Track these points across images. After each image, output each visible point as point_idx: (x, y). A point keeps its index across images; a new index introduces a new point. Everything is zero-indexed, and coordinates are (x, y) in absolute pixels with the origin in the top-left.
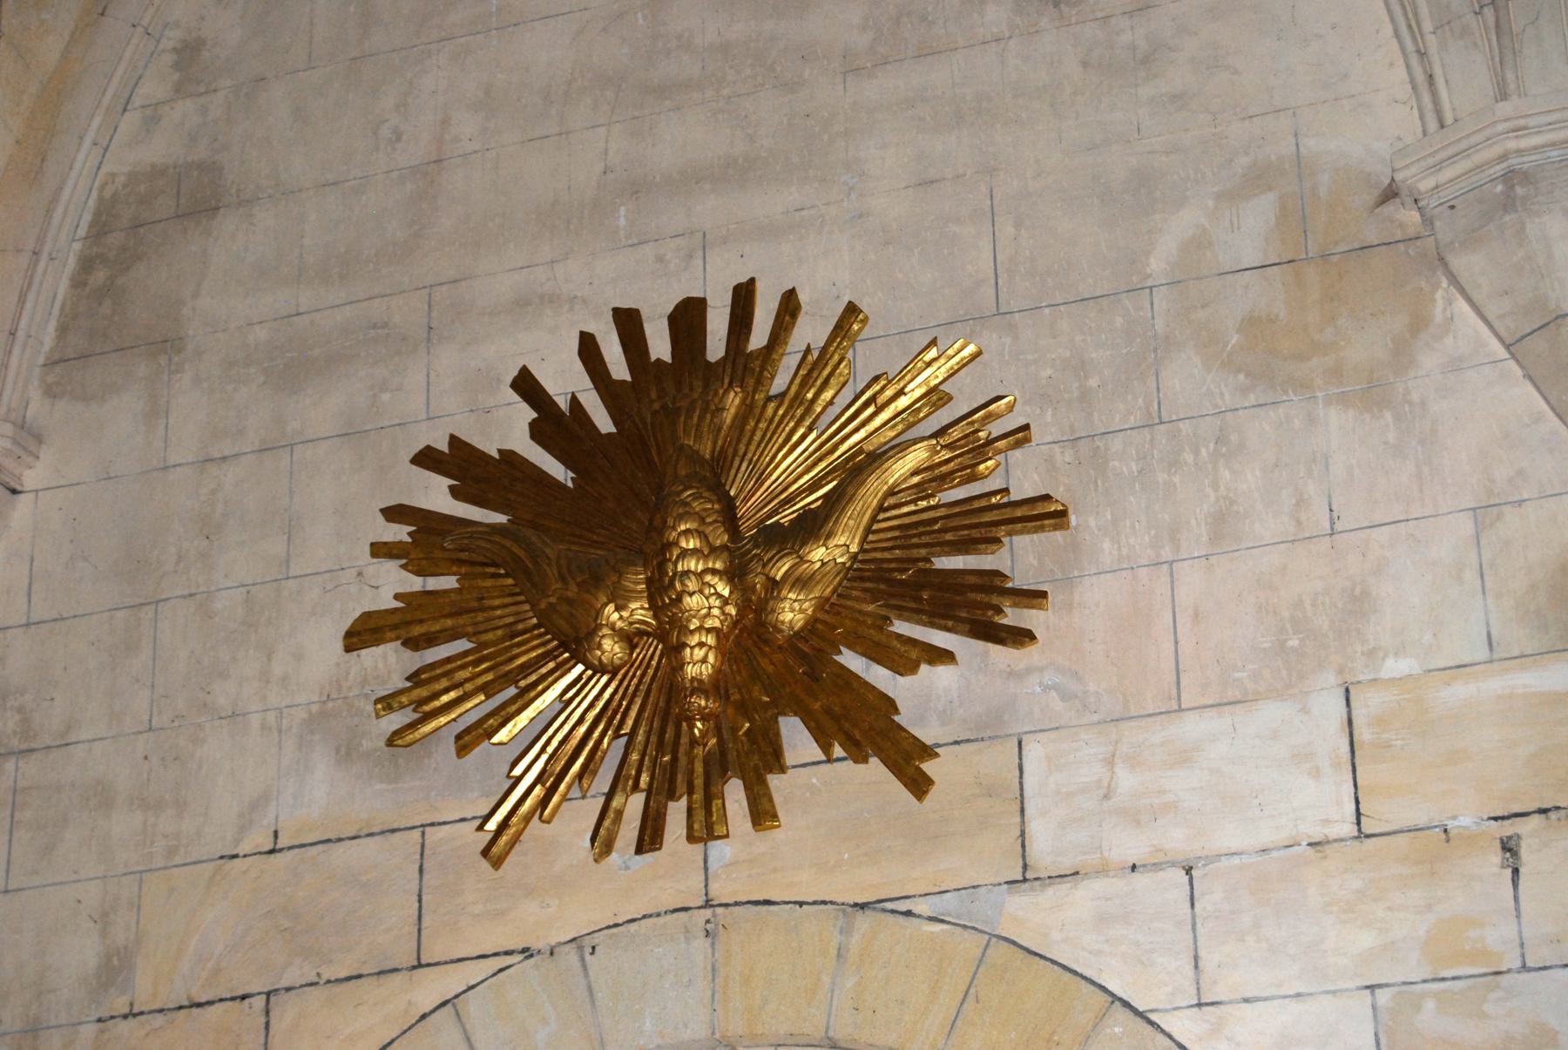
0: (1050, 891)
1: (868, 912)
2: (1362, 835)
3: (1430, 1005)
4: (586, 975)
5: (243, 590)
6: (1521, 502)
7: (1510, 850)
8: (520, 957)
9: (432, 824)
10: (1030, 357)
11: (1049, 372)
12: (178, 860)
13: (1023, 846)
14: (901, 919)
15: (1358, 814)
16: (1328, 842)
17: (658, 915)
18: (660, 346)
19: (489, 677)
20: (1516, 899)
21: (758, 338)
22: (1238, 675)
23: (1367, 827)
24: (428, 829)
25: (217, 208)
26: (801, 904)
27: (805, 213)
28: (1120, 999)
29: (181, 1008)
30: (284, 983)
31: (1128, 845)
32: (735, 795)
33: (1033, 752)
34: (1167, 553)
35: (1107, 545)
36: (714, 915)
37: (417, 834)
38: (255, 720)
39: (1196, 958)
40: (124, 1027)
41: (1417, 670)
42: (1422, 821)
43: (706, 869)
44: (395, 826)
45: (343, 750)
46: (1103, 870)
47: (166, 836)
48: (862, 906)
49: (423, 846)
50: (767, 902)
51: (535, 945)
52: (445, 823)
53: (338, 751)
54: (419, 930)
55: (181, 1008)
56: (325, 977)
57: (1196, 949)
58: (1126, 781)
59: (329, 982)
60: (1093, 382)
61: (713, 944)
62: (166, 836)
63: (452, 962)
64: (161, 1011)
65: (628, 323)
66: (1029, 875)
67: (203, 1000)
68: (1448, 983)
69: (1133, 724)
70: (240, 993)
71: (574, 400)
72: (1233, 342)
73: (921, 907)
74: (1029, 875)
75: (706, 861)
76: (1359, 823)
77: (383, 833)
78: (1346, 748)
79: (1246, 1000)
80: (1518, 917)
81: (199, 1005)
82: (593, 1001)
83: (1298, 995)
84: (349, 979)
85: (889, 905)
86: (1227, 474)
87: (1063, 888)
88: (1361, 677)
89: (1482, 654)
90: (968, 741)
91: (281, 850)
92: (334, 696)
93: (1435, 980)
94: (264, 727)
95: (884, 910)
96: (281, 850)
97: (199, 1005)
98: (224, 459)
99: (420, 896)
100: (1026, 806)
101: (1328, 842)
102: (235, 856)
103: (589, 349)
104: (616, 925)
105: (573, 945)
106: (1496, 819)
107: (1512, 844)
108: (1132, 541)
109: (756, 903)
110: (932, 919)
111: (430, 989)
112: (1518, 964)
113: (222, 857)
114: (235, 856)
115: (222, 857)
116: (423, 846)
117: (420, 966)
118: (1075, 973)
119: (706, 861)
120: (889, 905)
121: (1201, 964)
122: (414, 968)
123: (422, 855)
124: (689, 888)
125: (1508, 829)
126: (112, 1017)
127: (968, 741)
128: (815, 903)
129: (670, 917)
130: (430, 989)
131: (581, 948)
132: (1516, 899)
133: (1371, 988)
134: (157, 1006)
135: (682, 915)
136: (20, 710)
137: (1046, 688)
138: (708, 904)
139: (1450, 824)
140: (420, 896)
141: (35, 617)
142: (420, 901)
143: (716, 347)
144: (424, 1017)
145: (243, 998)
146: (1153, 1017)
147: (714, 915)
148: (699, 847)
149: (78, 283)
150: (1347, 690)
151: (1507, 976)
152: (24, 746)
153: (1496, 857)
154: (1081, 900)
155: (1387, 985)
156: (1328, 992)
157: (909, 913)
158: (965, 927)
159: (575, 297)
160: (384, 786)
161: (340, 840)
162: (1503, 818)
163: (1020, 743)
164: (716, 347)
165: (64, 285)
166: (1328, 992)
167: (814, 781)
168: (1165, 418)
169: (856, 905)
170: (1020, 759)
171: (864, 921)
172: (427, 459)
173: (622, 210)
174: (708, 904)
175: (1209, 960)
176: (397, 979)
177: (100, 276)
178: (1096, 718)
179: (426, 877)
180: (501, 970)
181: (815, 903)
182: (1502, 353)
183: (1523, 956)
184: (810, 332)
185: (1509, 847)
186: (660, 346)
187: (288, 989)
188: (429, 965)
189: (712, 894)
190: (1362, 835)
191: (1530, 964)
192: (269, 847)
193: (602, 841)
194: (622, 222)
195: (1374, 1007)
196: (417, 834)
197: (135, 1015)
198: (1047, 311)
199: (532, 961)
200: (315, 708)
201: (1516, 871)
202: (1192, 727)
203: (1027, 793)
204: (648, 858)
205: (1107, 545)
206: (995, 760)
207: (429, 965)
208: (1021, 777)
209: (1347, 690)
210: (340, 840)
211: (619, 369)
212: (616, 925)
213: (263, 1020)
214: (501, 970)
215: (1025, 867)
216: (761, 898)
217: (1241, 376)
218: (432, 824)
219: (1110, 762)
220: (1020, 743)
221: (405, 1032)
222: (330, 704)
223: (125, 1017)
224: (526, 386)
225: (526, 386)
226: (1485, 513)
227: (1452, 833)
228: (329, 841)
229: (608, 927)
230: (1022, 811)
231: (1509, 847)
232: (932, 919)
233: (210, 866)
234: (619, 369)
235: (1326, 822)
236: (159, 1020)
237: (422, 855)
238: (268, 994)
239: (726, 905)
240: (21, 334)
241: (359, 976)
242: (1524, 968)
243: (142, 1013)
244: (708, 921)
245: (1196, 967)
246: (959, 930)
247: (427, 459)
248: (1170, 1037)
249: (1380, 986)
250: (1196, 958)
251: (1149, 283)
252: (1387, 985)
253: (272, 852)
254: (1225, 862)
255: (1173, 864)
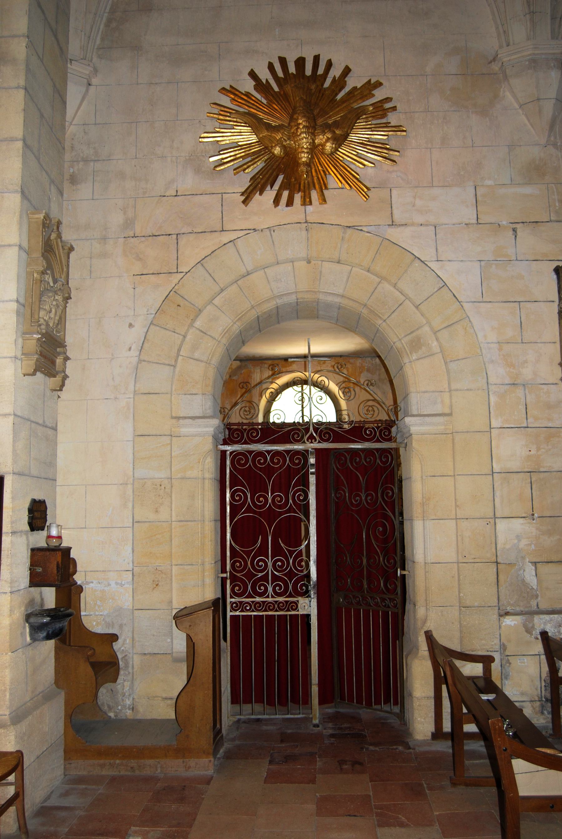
0: (399, 229)
1: (350, 229)
2: (478, 223)
3: (494, 266)
4: (272, 238)
5: (164, 122)
6: (520, 146)
7: (515, 231)
8: (253, 231)
9: (225, 193)
10: (393, 88)
11: (399, 93)
12: (147, 196)
13: (392, 216)
14: (360, 232)
15: (477, 218)
16: (470, 224)
17: (292, 224)
18: (292, 69)
19: (243, 154)
20: (515, 243)
21: (321, 71)
22: (448, 179)
23: (480, 221)
24: (223, 194)
25: (151, 10)
26: (332, 225)
27: (331, 39)
28: (418, 257)
29: (150, 236)
30: (182, 232)
31: (419, 219)
32: (314, 195)
33: (394, 192)
34: (429, 146)
35: (414, 141)
36: (308, 225)
37: (220, 195)
38: (169, 159)
39: (437, 249)
40: (132, 240)
41: (493, 184)
42: (493, 221)
43: (305, 213)
44: (213, 192)
45: (197, 170)
46: (413, 224)
47: (143, 189)
48: (349, 227)
49: (222, 198)
50: (322, 223)
51: (257, 229)
52: (228, 193)
53: (195, 170)
54: (222, 221)
55: (150, 236)
56: (195, 231)
57: (437, 247)
58: (418, 202)
59: (196, 233)
60: (411, 98)
61: (308, 233)
62: (143, 189)
63: (233, 230)
64: (144, 236)
65: (283, 61)
66: (394, 224)
67: (157, 234)
68: (499, 262)
69: (420, 188)
70: (168, 233)
71: (267, 80)
72: (448, 93)
73: (365, 229)
74: (394, 224)
75: (305, 211)
76: (477, 220)
77: (210, 194)
78: (475, 201)
79: (449, 261)
80: (516, 247)
81: (155, 236)
82: (274, 245)
83: (462, 261)
84: (202, 232)
85: (356, 228)
86: (446, 128)
87: (402, 228)
88: (479, 184)
89: (509, 182)
90: (377, 188)
91: (179, 196)
92: (193, 155)
93: (495, 260)
94: (172, 161)
95: (355, 229)
96: (179, 196)
97: (155, 236)
98: (156, 84)
99: (222, 212)
100: (393, 206)
101: (470, 224)
102: (165, 196)
103: (271, 67)
104: (280, 225)
105: (268, 229)
106: (511, 223)
107: (515, 229)
108: (420, 141)
109: (320, 223)
110: (368, 232)
111: (226, 237)
112: (515, 259)
113: (160, 196)
114: (165, 196)
115: (160, 196)
116: (222, 198)
117: (223, 231)
118: (406, 250)
119: (305, 211)
120: (356, 228)
121: (438, 251)
122: (221, 231)
123: (222, 201)
124: (301, 217)
125: (514, 226)
126: (129, 237)
127: (377, 188)
128: (336, 225)
129: (295, 224)
130: (226, 237)
131: (270, 231)
132: (515, 243)
133: (480, 261)
134: (143, 235)
135: (299, 224)
136: (94, 148)
137: (397, 176)
138: (306, 222)
139: (500, 223)
140: (222, 212)
141: (97, 122)
142: (222, 213)
143: (308, 71)
144: (225, 244)
145: (169, 235)
146: (426, 262)
147: (308, 225)
148: (304, 207)
149: (107, 25)
150: (475, 187)
151: (512, 262)
152: (96, 159)
153: (511, 232)
154: (408, 231)
155: (484, 261)
156: (469, 261)
157: (361, 230)
158: (377, 235)
159: (264, 52)
160: (210, 181)
161: (197, 195)
162: (513, 223)
163: (391, 190)
164: (308, 71)
165: (102, 27)
166: (469, 261)
167: (335, 193)
168: (430, 110)
169: (347, 226)
170: (391, 193)
171: (349, 231)
172: (223, 90)
173: (277, 30)
174: (306, 222)
175: (440, 250)
176: (216, 234)
177: (114, 25)
178: (411, 186)
179: (223, 207)
180: (247, 234)
181: (336, 225)
182: (517, 107)
183: (517, 257)
184: (336, 72)
185: (514, 230)
186: (292, 69)
187: (183, 234)
188: (226, 231)
189: (307, 219)
190: (478, 223)
191: (518, 259)
192: (176, 194)
193: (276, 202)
194: (277, 33)
195: (481, 266)
196: (220, 195)
197: (136, 237)
198: (399, 77)
199: (256, 232)
200: (187, 158)
201: (516, 236)
202: (436, 191)
203: (393, 203)
204: (289, 208)
205: (414, 141)
206: (384, 193)
207: (226, 231)
208: (391, 198)
209: (475, 187)
210: (197, 195)
211: (280, 74)
212: (280, 225)
213: (176, 241)
214: (247, 234)
215: (393, 222)
216: (321, 222)
217: (450, 103)
218: (225, 193)
219: (415, 198)
220: (391, 190)
221: (219, 248)
222: (192, 157)
223: (133, 237)
224: (253, 75)
225: (253, 75)
226: (511, 147)
227: (501, 225)
228: (194, 194)
229: (278, 225)
230: (392, 207)
231: (514, 230)
232: (368, 232)
233: (157, 198)
234: (280, 74)
235: (469, 219)
236: (143, 239)
237: (222, 201)
238: (177, 235)
239: (311, 223)
240: (91, 37)
241: (205, 232)
242: (517, 260)
243: (138, 237)
244: (306, 227)
245: (437, 251)
246: (375, 236)
247: (223, 90)
248: (430, 268)
249: (482, 261)
250: (437, 249)
251: (426, 74)
252: (484, 261)
253: (176, 196)
254: (444, 226)
255: (431, 225)
